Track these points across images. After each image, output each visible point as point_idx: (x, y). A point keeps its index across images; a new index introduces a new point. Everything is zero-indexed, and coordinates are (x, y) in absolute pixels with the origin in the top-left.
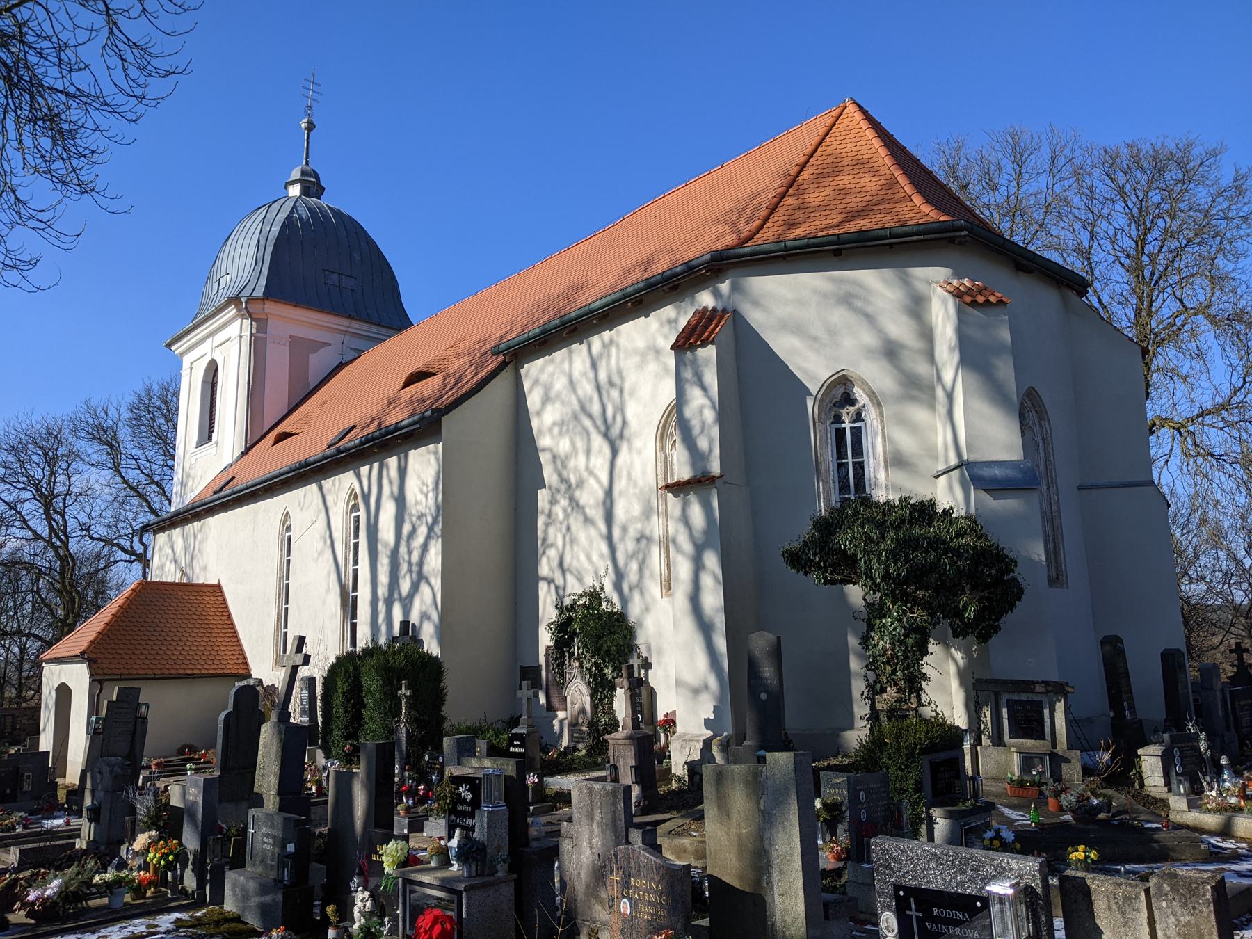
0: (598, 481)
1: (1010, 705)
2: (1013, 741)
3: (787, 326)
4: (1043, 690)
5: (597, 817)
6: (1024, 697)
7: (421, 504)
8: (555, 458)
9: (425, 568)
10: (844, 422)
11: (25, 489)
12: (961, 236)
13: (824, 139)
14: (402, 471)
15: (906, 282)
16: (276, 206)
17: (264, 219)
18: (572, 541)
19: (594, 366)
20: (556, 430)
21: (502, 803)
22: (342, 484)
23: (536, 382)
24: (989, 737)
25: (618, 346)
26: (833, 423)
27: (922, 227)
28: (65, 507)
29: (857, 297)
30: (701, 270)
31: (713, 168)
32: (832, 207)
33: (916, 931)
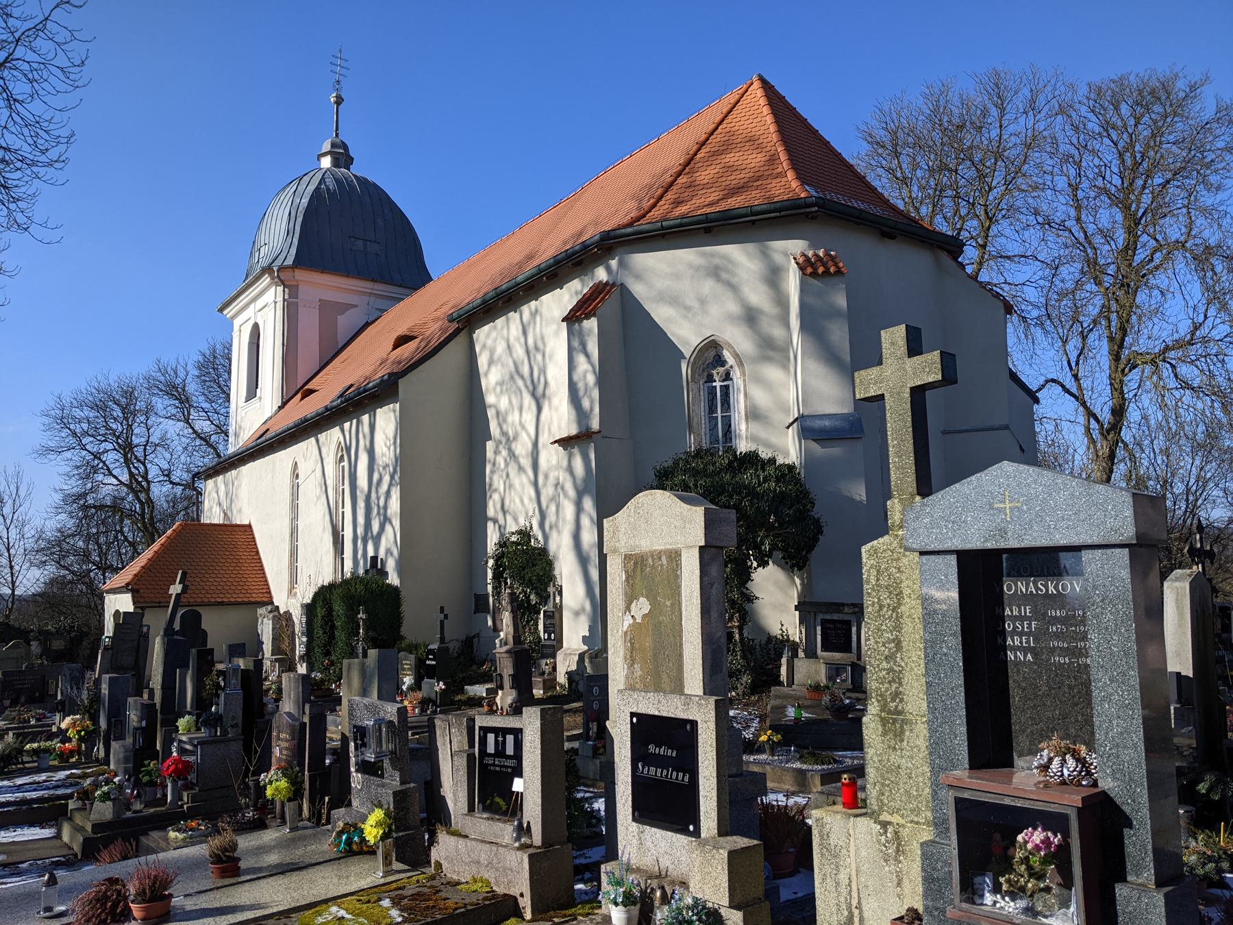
0: (528, 435)
1: (824, 623)
2: (824, 653)
3: (663, 298)
4: (851, 611)
5: (292, 696)
6: (836, 617)
7: (386, 456)
8: (498, 413)
9: (389, 512)
10: (715, 381)
11: (105, 441)
12: (812, 212)
13: (726, 116)
14: (372, 427)
15: (765, 255)
16: (306, 179)
17: (295, 191)
18: (511, 486)
19: (525, 333)
20: (498, 389)
21: (239, 687)
22: (332, 437)
23: (484, 346)
24: (804, 651)
25: (541, 315)
26: (706, 382)
27: (779, 205)
28: (146, 455)
29: (727, 271)
30: (594, 248)
31: (651, 140)
32: (718, 184)
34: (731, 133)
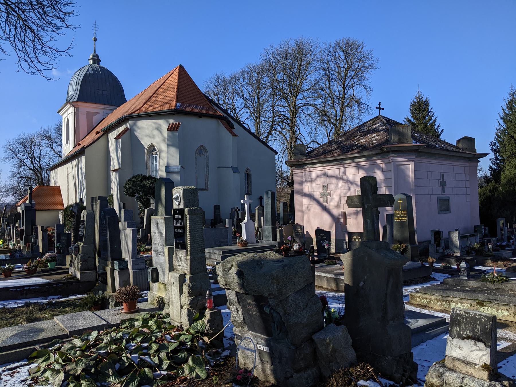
16: (83, 69)
22: (74, 162)
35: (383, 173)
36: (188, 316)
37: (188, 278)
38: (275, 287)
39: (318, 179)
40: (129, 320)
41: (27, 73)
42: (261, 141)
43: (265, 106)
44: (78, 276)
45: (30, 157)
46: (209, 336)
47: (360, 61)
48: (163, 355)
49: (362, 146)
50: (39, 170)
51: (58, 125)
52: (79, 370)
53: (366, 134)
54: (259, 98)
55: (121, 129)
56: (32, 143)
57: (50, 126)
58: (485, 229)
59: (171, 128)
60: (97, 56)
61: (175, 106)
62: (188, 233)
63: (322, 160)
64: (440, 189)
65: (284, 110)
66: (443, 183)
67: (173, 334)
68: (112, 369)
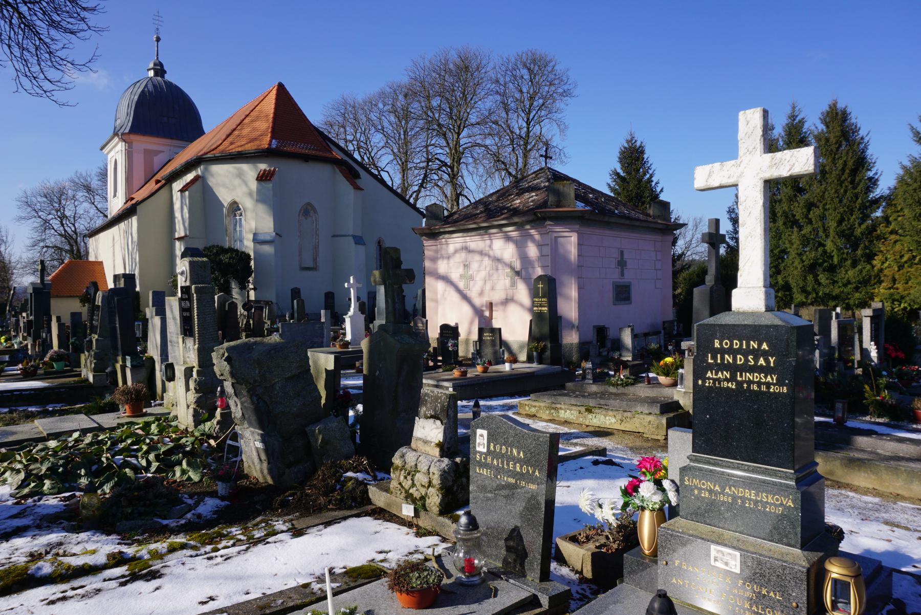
16: (138, 84)
22: (122, 225)
33: (119, 336)
34: (261, 111)
35: (538, 249)
36: (194, 416)
37: (195, 370)
38: (257, 372)
39: (457, 255)
40: (127, 423)
41: (30, 94)
42: (407, 202)
43: (414, 145)
44: (91, 379)
45: (59, 217)
46: (215, 439)
47: (551, 84)
48: (152, 457)
49: (515, 209)
50: (74, 237)
51: (103, 168)
52: (44, 469)
53: (523, 193)
54: (405, 132)
55: (189, 177)
56: (61, 195)
57: (90, 170)
58: (678, 327)
59: (262, 177)
60: (161, 65)
61: (270, 144)
62: (196, 317)
63: (462, 227)
64: (617, 271)
65: (442, 153)
66: (622, 264)
67: (174, 436)
68: (85, 470)
